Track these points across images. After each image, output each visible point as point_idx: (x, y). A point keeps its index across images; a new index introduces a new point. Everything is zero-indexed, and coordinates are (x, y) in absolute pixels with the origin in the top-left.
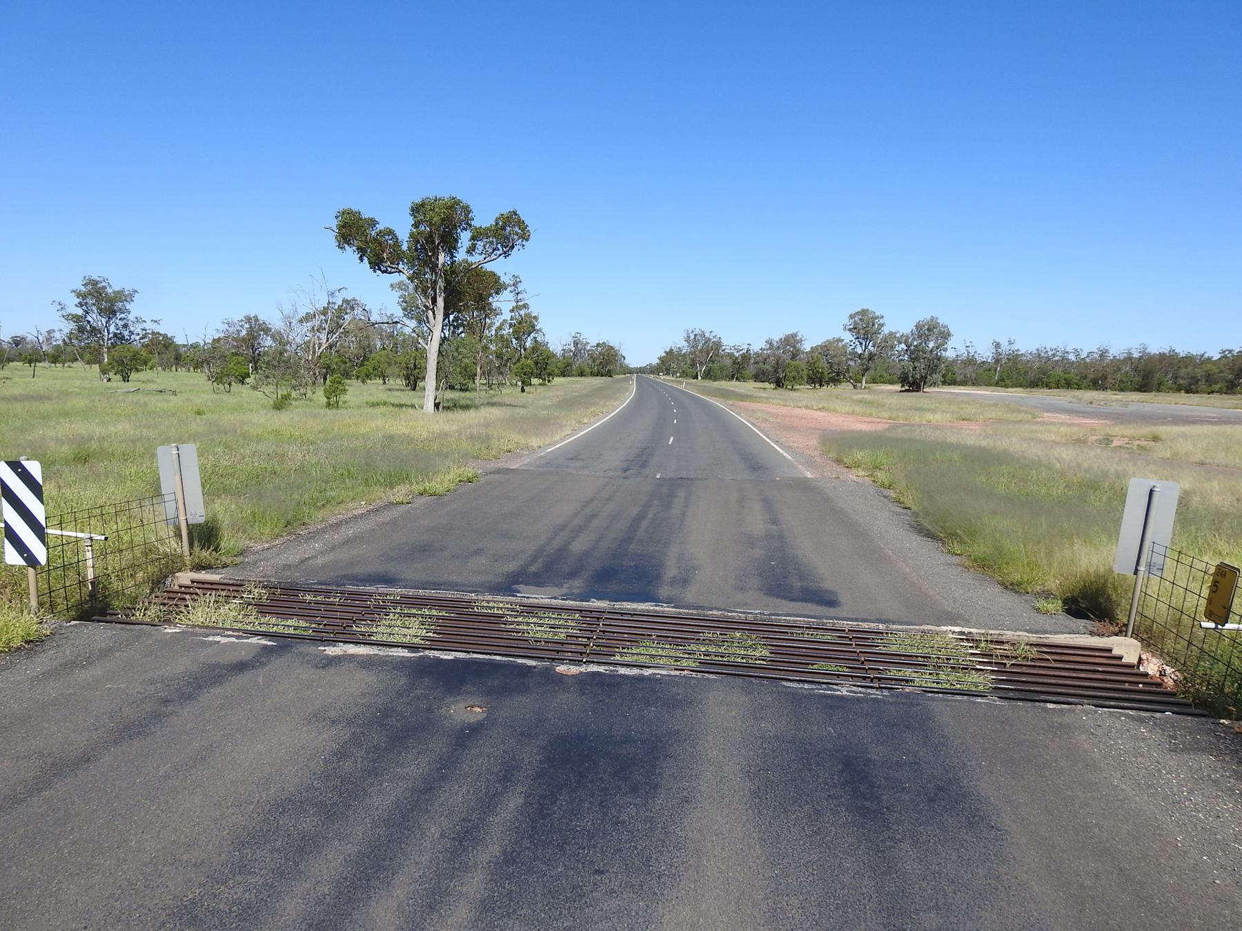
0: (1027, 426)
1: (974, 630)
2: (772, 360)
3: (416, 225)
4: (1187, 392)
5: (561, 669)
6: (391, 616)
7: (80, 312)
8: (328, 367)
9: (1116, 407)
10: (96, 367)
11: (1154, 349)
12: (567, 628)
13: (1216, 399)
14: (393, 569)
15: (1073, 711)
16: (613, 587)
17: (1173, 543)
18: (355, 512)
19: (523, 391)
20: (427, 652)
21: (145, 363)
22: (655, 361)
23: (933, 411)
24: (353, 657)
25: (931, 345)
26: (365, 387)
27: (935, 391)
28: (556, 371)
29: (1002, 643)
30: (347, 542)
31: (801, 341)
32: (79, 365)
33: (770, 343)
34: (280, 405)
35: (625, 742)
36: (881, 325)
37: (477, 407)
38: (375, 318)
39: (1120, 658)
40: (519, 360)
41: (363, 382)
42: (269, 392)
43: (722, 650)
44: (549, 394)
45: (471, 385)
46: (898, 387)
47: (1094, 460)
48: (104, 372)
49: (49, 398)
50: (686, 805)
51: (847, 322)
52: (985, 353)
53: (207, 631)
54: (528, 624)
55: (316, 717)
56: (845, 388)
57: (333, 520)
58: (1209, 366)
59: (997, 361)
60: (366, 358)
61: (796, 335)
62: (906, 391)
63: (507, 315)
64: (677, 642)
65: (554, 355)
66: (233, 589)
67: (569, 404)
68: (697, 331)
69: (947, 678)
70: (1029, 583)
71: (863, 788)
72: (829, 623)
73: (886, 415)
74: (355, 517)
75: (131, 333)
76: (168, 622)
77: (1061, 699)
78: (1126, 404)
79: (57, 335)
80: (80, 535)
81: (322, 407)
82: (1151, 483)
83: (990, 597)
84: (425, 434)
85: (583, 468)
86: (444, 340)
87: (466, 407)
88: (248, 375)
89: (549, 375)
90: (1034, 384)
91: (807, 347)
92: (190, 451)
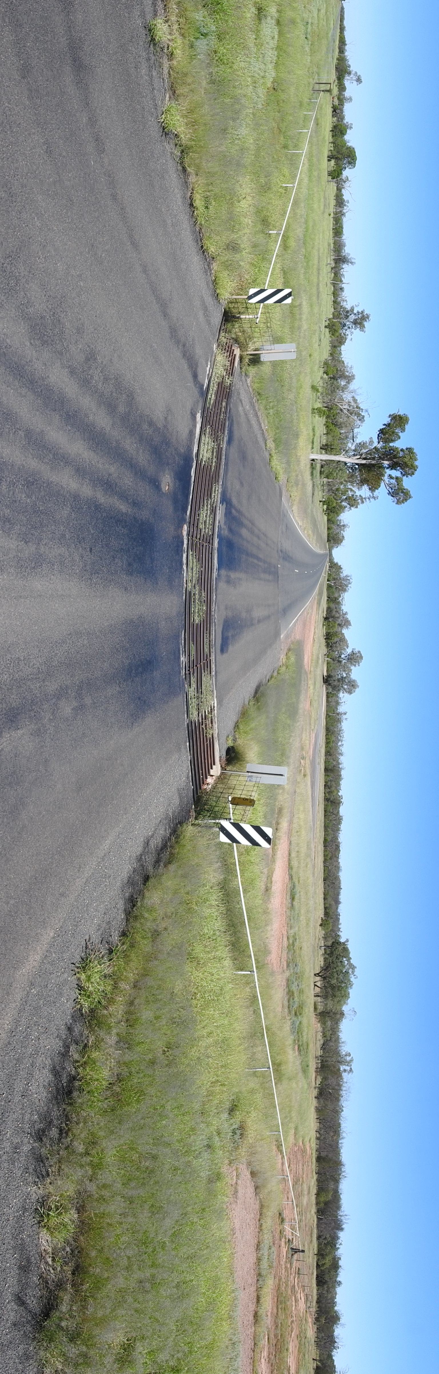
0: (308, 727)
1: (216, 711)
2: (337, 615)
3: (402, 450)
4: (325, 785)
5: (185, 527)
6: (213, 444)
7: (355, 311)
8: (331, 409)
9: (317, 760)
10: (331, 316)
11: (343, 773)
12: (205, 529)
13: (322, 796)
14: (235, 443)
15: (187, 752)
16: (224, 549)
17: (262, 784)
18: (262, 424)
19: (320, 501)
20: (195, 462)
21: (333, 335)
22: (336, 561)
23: (314, 688)
24: (195, 426)
25: (346, 687)
26: (322, 425)
27: (323, 690)
28: (330, 517)
29: (212, 723)
30: (248, 420)
31: (347, 628)
32: (333, 310)
33: (346, 613)
34: (314, 388)
35: (151, 559)
36: (355, 666)
37: (312, 479)
38: (356, 430)
39: (212, 768)
40: (335, 499)
41: (325, 425)
42: (320, 384)
43: (197, 601)
44: (319, 514)
45: (323, 476)
46: (325, 674)
47: (294, 755)
48: (329, 319)
49: (318, 299)
50: (123, 590)
51: (356, 650)
52: (341, 709)
53: (212, 362)
54: (207, 510)
55: (169, 410)
56: (324, 650)
57: (259, 414)
58: (336, 792)
59: (338, 714)
60: (336, 425)
61: (350, 625)
62: (324, 678)
63: (358, 493)
64: (199, 580)
65: (338, 516)
66: (231, 372)
67: (315, 524)
68: (351, 581)
69: (193, 703)
70: (239, 733)
71: (140, 669)
72: (213, 650)
73: (312, 669)
74: (260, 424)
75: (346, 330)
76: (219, 346)
77: (191, 748)
78: (319, 764)
79: (345, 303)
80: (259, 314)
81: (313, 406)
82: (286, 775)
83: (232, 717)
84: (299, 454)
85: (282, 532)
86: (346, 464)
87: (312, 474)
88: (327, 375)
89: (328, 514)
90: (328, 729)
91: (344, 631)
92: (293, 356)
